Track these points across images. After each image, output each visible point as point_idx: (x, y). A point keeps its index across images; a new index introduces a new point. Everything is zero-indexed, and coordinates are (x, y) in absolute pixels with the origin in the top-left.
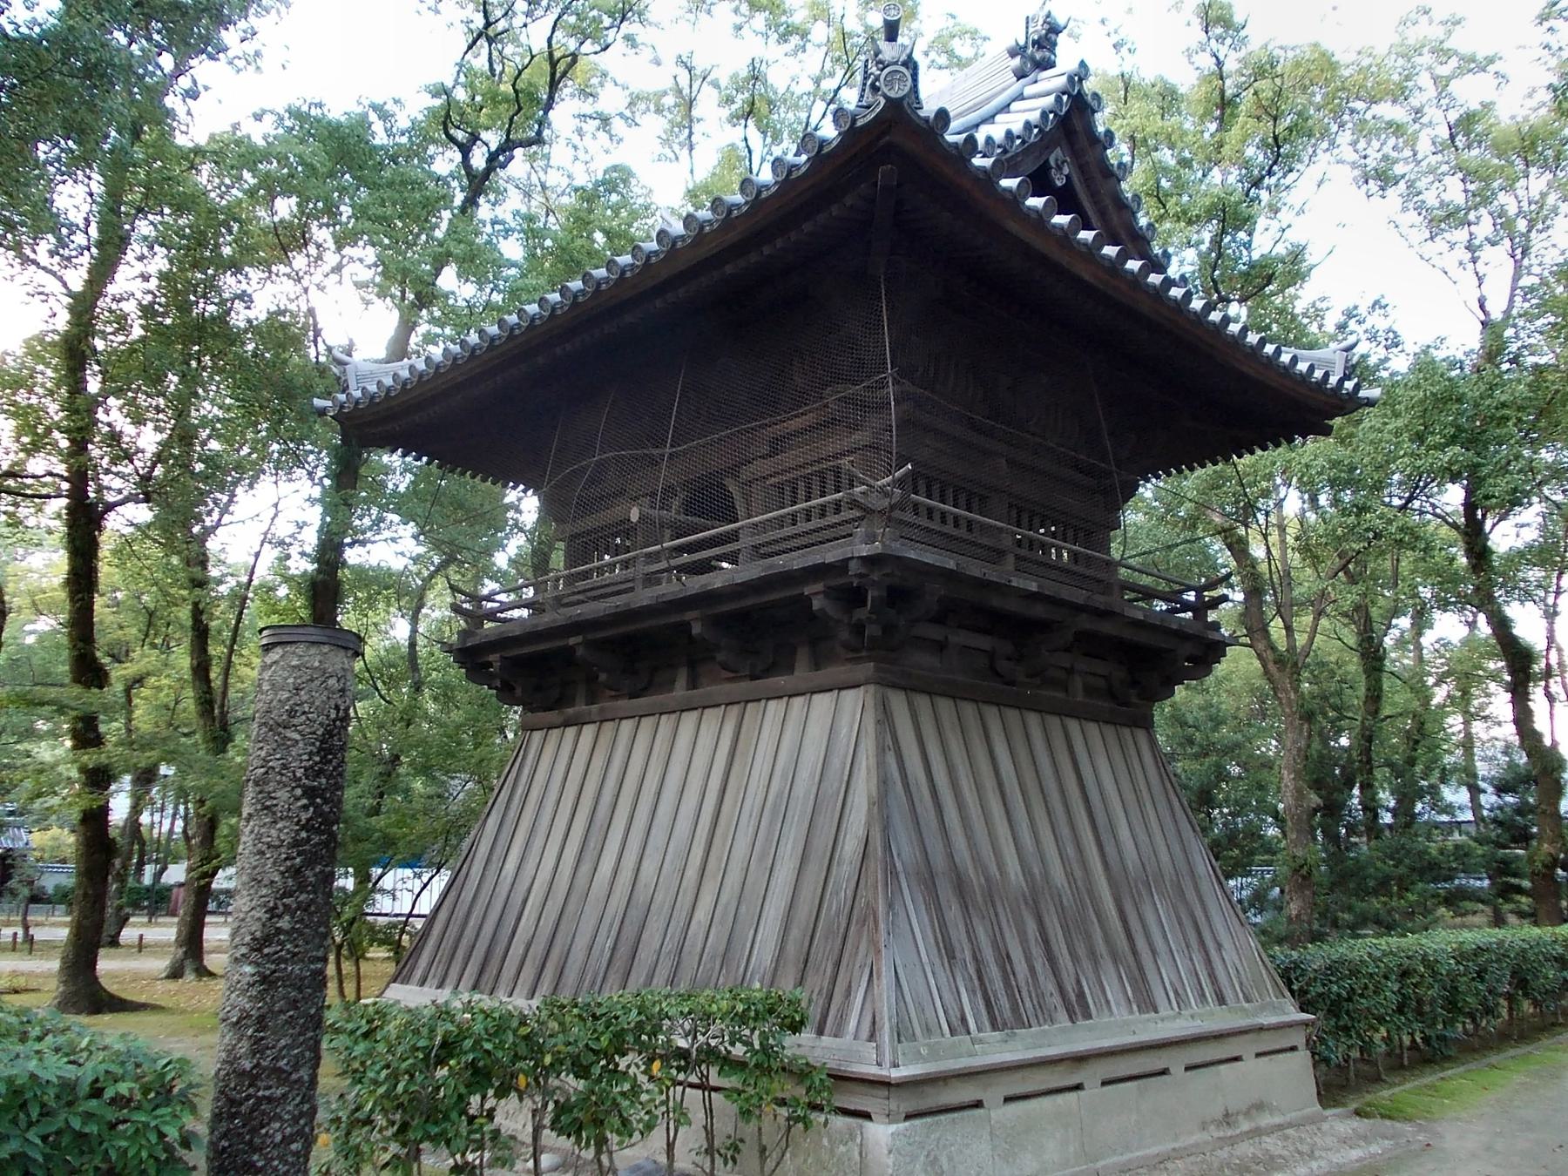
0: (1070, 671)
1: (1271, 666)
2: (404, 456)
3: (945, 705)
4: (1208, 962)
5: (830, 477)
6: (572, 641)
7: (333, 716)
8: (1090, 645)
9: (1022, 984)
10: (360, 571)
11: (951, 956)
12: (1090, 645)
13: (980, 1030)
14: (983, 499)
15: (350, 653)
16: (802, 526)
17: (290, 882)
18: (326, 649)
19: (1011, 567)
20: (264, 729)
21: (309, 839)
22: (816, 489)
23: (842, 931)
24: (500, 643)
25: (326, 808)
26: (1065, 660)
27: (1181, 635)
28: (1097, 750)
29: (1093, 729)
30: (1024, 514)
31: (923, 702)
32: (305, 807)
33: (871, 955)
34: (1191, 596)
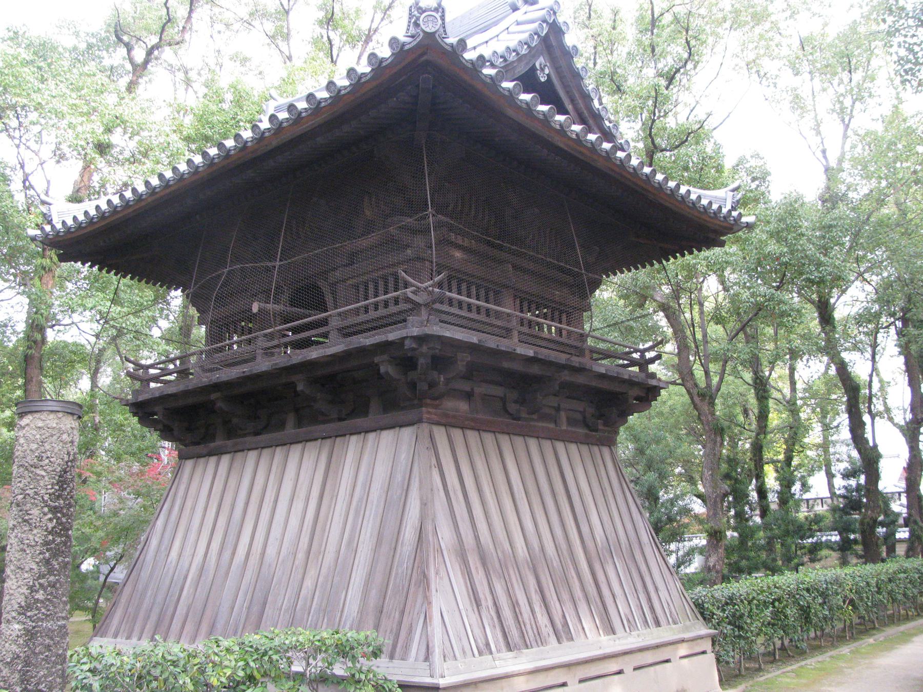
0: (558, 409)
1: (697, 399)
2: (91, 267)
3: (472, 435)
4: (649, 599)
5: (391, 280)
6: (213, 396)
7: (66, 459)
8: (572, 391)
9: (527, 621)
10: (54, 351)
11: (478, 604)
12: (572, 391)
13: (499, 651)
14: (497, 293)
15: (75, 417)
16: (372, 314)
17: (43, 569)
18: (60, 415)
19: (516, 340)
20: (22, 469)
21: (54, 540)
22: (381, 288)
23: (405, 590)
24: (163, 399)
25: (64, 520)
26: (553, 401)
27: (631, 383)
28: (575, 463)
29: (573, 447)
30: (526, 301)
31: (457, 433)
32: (51, 520)
33: (425, 605)
34: (636, 356)
